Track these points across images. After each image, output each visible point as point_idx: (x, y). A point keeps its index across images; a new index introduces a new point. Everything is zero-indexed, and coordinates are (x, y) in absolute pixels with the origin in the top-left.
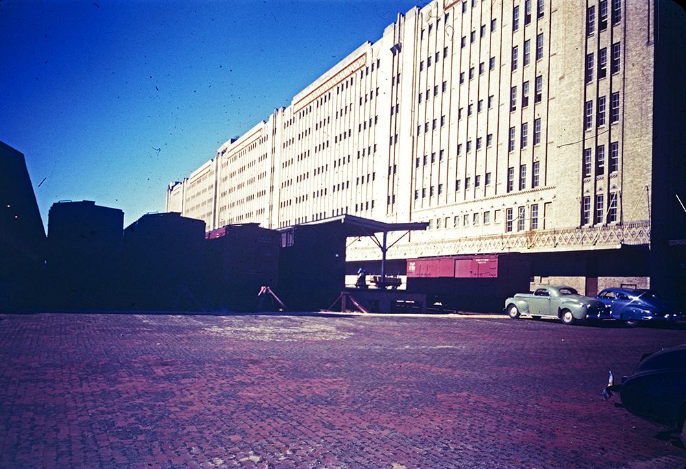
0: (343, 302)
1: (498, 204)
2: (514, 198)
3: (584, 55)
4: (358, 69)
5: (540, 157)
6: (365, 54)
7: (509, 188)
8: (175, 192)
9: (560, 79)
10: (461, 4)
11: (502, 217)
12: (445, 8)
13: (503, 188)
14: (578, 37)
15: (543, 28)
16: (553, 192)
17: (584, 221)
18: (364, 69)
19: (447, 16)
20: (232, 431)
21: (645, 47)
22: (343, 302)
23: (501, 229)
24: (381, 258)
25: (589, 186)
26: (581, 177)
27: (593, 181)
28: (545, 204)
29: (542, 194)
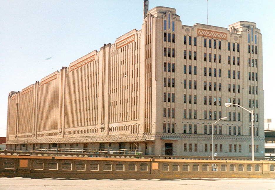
18: (133, 42)
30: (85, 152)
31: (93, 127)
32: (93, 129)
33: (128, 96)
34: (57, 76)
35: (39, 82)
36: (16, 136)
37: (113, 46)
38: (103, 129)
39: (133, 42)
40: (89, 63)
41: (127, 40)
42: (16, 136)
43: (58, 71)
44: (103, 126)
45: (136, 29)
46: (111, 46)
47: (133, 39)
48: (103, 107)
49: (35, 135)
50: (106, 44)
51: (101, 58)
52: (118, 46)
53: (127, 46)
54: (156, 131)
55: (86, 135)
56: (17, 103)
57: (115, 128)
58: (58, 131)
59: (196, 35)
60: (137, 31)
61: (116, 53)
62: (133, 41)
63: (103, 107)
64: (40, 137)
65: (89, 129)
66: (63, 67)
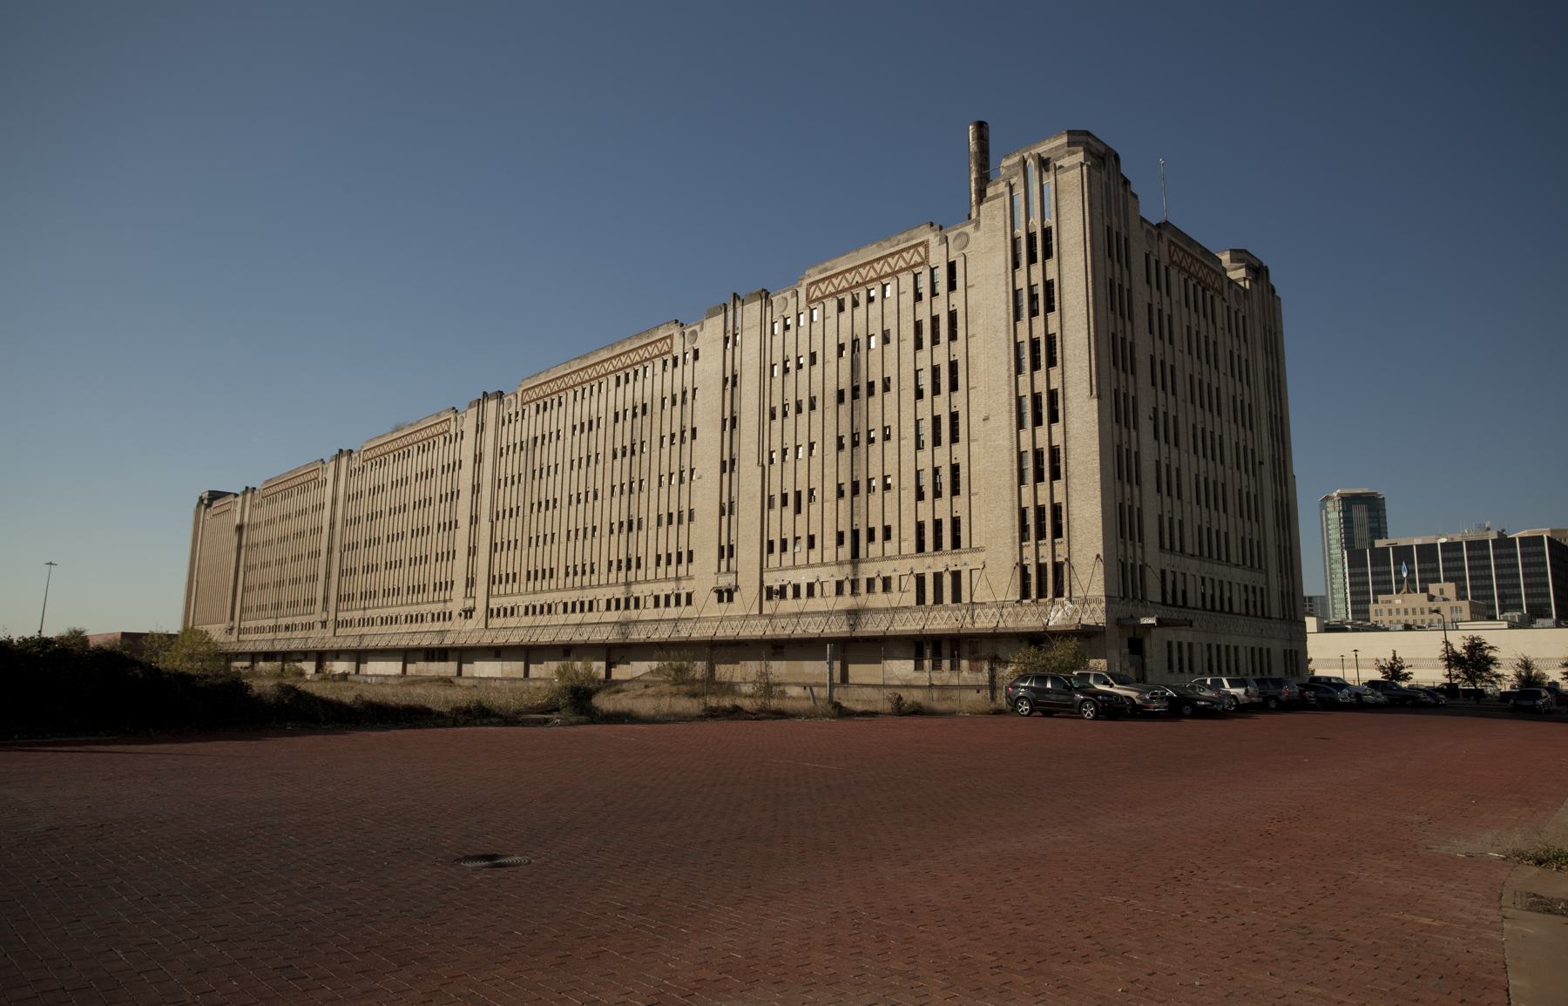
0: (1476, 553)
1: (904, 567)
2: (928, 561)
3: (1014, 397)
4: (831, 295)
5: (963, 515)
6: (671, 337)
7: (920, 547)
8: (217, 511)
9: (984, 420)
10: (835, 302)
11: (911, 585)
12: (364, 461)
13: (909, 545)
14: (1005, 374)
15: (957, 354)
16: (982, 556)
17: (1025, 594)
18: (447, 435)
19: (524, 410)
20: (1543, 831)
21: (1087, 400)
22: (1476, 553)
23: (910, 598)
24: (532, 667)
25: (1029, 552)
26: (1017, 540)
27: (1033, 547)
28: (971, 570)
29: (966, 557)
30: (1064, 677)
31: (304, 619)
32: (271, 625)
33: (429, 548)
34: (320, 475)
35: (254, 489)
36: (232, 629)
37: (357, 455)
38: (324, 624)
39: (447, 435)
40: (306, 485)
41: (425, 435)
42: (232, 629)
43: (322, 460)
44: (469, 603)
45: (454, 408)
46: (505, 399)
47: (666, 348)
48: (328, 575)
49: (330, 625)
50: (489, 393)
51: (330, 476)
52: (366, 458)
53: (588, 388)
54: (1106, 590)
55: (256, 636)
56: (238, 521)
57: (385, 619)
58: (318, 616)
59: (1165, 261)
60: (457, 411)
61: (260, 505)
62: (446, 431)
63: (328, 575)
64: (251, 635)
65: (297, 623)
66: (247, 488)
